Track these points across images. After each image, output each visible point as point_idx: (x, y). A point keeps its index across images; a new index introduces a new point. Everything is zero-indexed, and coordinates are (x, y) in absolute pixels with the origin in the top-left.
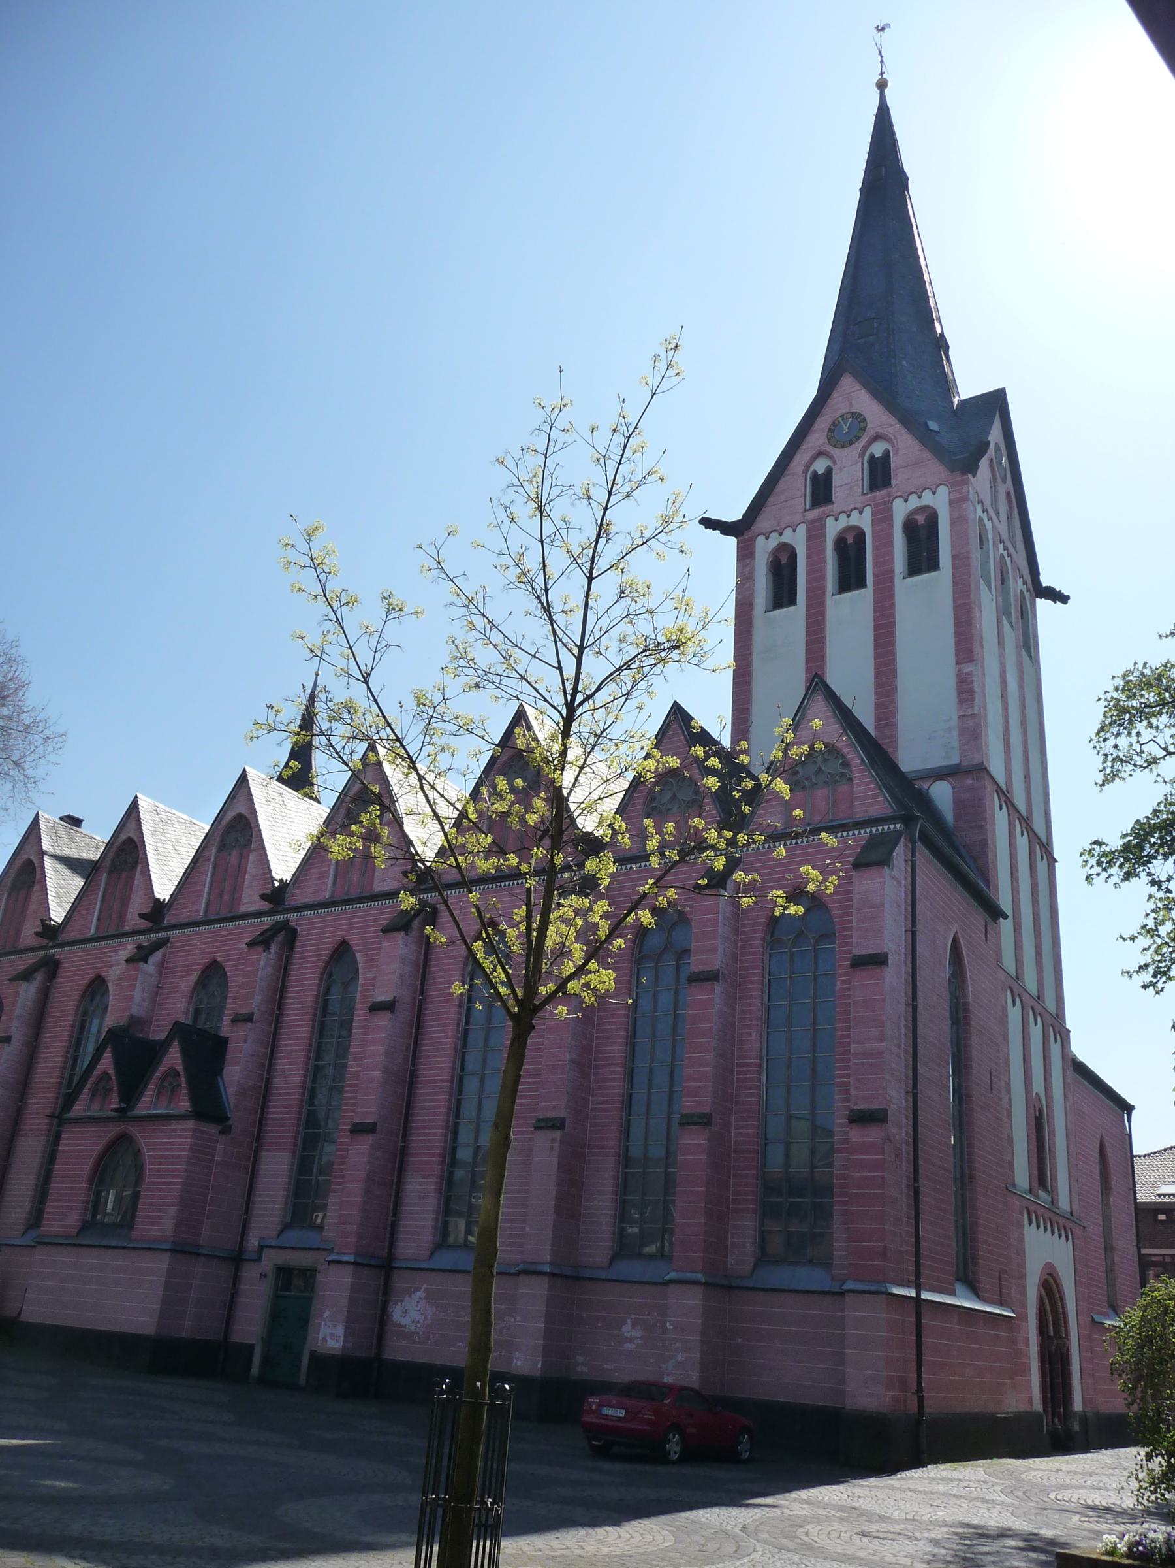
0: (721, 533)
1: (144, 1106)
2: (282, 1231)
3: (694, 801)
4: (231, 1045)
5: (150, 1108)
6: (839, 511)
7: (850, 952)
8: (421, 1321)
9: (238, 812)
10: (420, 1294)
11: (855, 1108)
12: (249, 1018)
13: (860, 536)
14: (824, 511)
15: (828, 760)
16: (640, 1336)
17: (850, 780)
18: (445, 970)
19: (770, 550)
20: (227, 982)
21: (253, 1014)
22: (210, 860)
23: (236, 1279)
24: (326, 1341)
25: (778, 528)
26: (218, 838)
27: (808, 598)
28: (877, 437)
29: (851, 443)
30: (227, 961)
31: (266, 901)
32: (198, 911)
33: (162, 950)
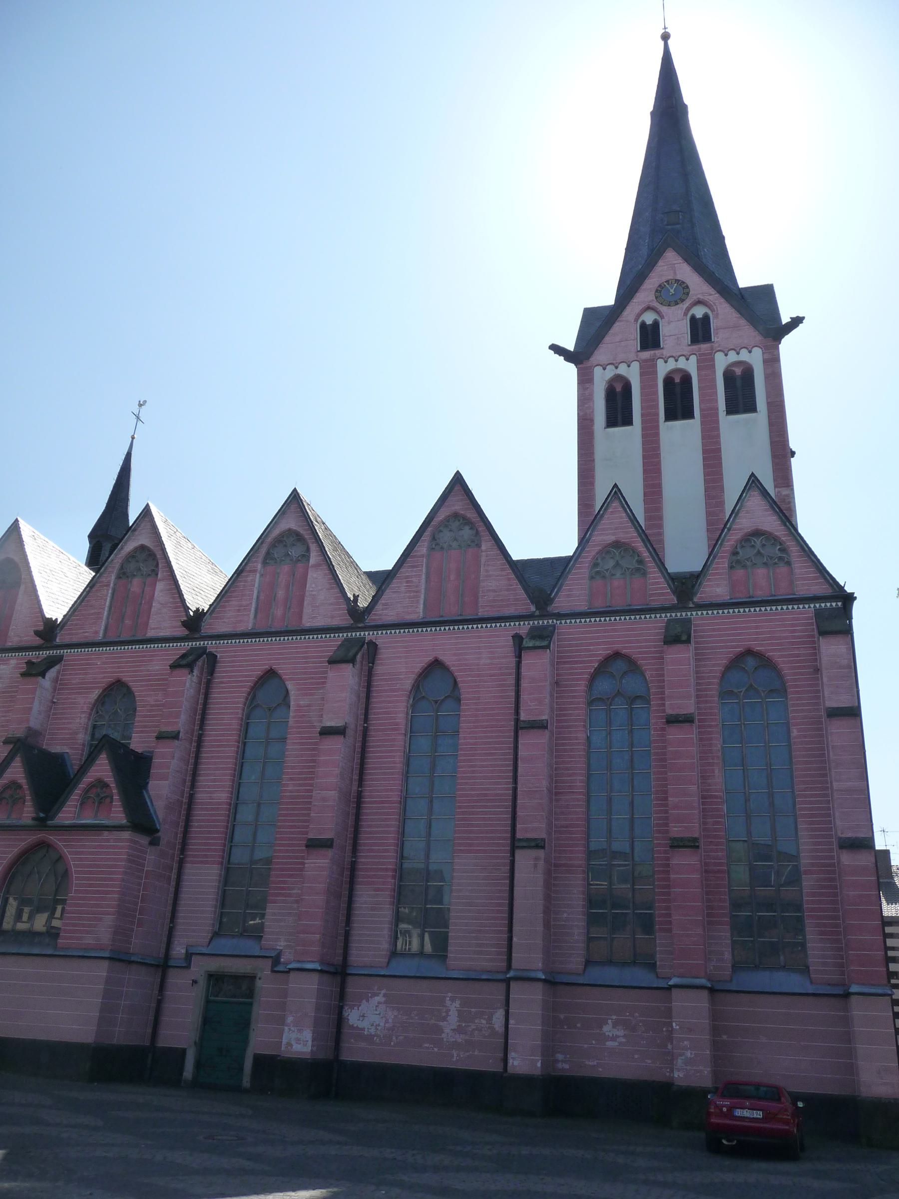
0: (565, 359)
1: (68, 814)
2: (211, 939)
3: (638, 570)
4: (155, 761)
5: (74, 818)
6: (668, 355)
7: (664, 711)
8: (382, 1024)
9: (140, 543)
10: (380, 998)
11: (843, 836)
12: (175, 736)
13: (686, 379)
14: (655, 353)
15: (744, 547)
16: (622, 1035)
17: (788, 563)
18: (389, 702)
19: (607, 379)
20: (135, 701)
21: (179, 732)
22: (108, 585)
23: (162, 987)
24: (291, 1045)
25: (614, 362)
26: (264, 550)
27: (643, 422)
28: (699, 302)
29: (677, 304)
30: (134, 681)
31: (185, 627)
32: (97, 633)
33: (57, 667)
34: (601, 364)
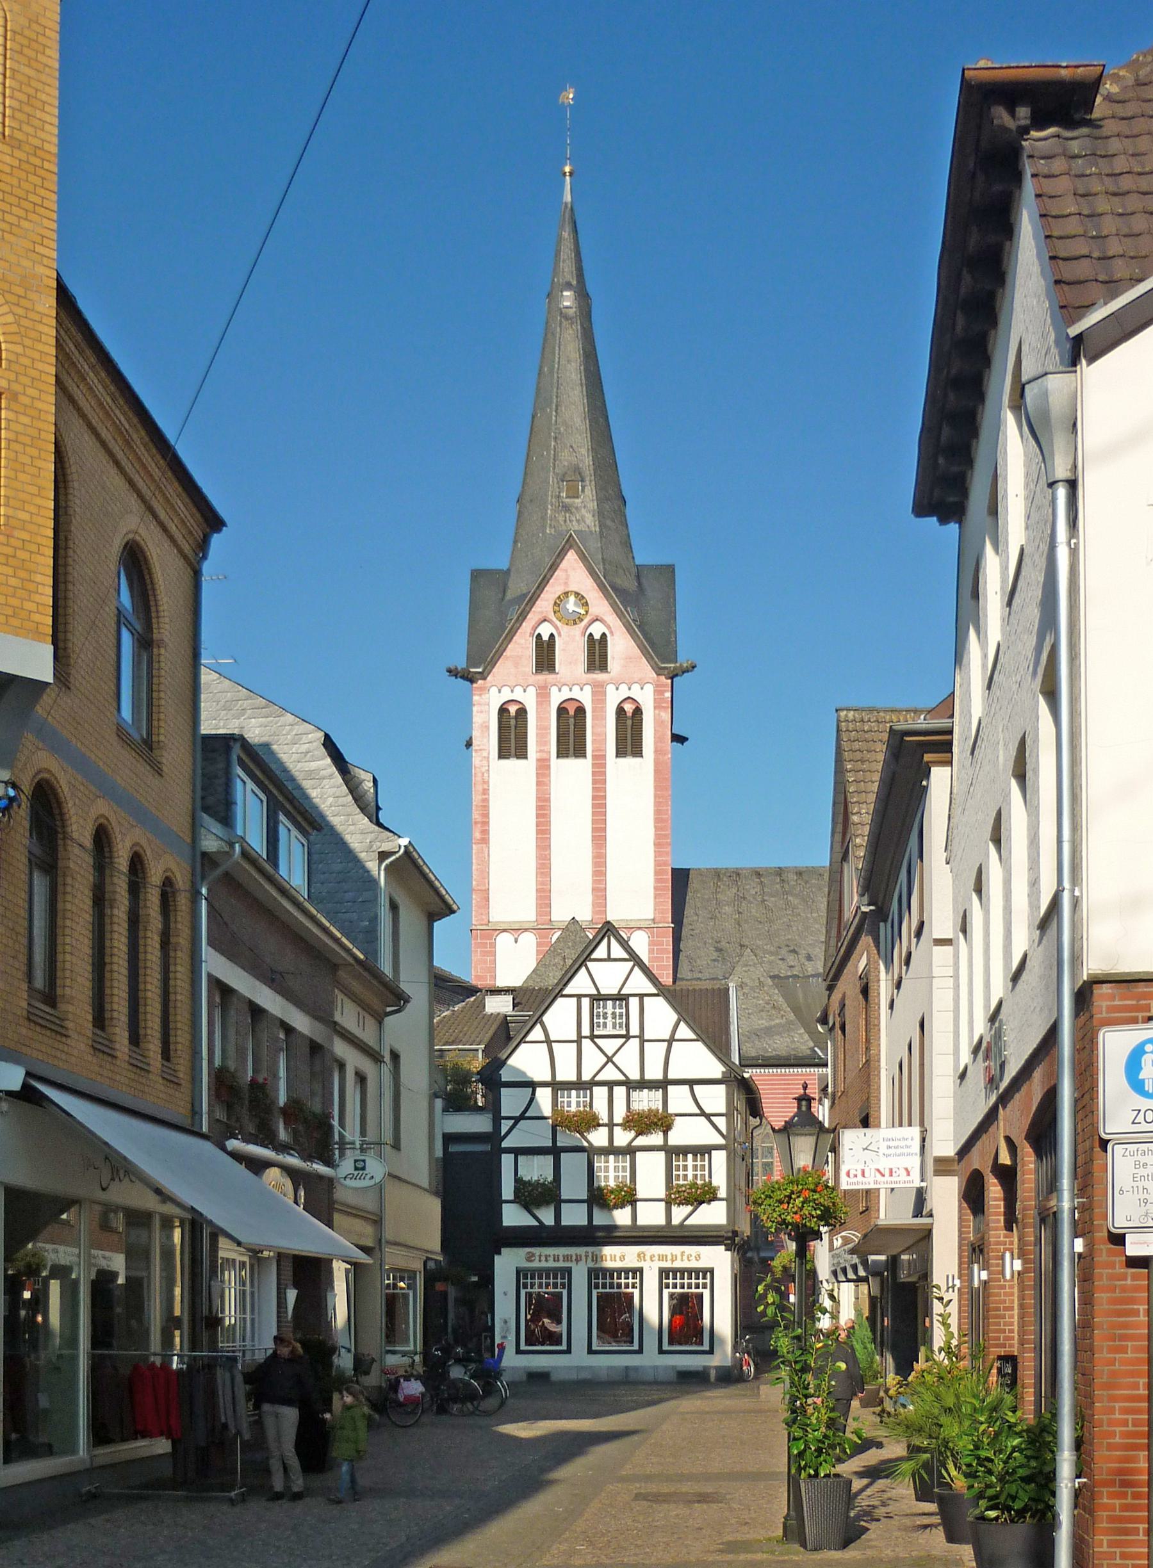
34: (636, 680)
